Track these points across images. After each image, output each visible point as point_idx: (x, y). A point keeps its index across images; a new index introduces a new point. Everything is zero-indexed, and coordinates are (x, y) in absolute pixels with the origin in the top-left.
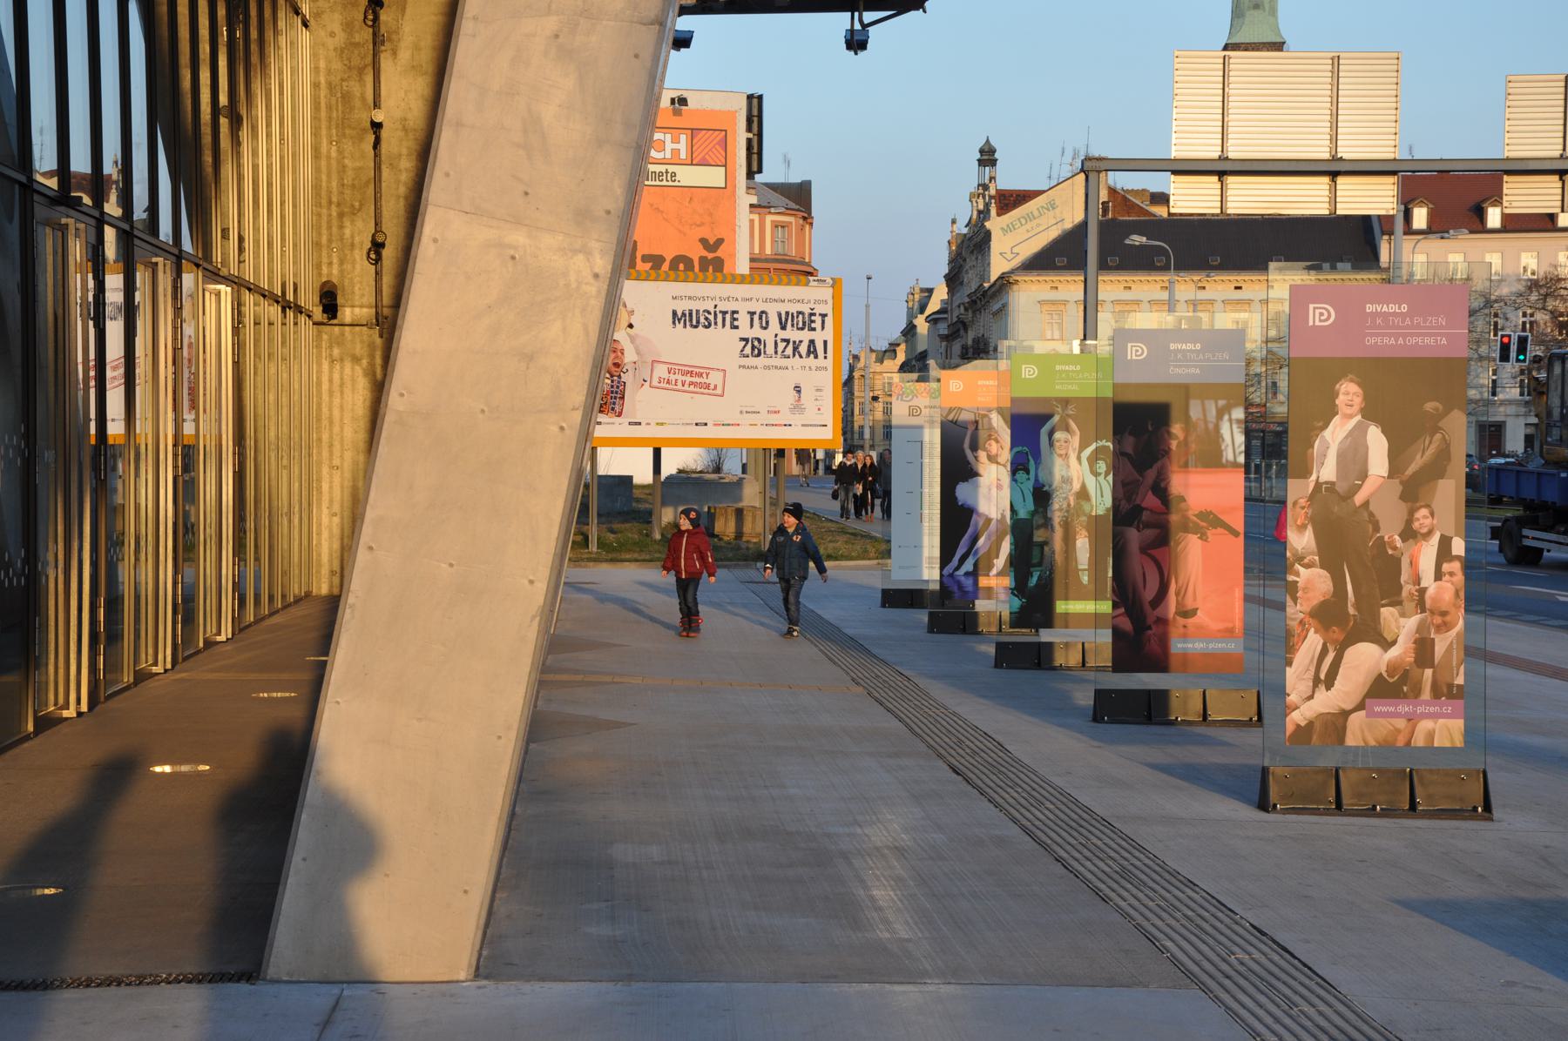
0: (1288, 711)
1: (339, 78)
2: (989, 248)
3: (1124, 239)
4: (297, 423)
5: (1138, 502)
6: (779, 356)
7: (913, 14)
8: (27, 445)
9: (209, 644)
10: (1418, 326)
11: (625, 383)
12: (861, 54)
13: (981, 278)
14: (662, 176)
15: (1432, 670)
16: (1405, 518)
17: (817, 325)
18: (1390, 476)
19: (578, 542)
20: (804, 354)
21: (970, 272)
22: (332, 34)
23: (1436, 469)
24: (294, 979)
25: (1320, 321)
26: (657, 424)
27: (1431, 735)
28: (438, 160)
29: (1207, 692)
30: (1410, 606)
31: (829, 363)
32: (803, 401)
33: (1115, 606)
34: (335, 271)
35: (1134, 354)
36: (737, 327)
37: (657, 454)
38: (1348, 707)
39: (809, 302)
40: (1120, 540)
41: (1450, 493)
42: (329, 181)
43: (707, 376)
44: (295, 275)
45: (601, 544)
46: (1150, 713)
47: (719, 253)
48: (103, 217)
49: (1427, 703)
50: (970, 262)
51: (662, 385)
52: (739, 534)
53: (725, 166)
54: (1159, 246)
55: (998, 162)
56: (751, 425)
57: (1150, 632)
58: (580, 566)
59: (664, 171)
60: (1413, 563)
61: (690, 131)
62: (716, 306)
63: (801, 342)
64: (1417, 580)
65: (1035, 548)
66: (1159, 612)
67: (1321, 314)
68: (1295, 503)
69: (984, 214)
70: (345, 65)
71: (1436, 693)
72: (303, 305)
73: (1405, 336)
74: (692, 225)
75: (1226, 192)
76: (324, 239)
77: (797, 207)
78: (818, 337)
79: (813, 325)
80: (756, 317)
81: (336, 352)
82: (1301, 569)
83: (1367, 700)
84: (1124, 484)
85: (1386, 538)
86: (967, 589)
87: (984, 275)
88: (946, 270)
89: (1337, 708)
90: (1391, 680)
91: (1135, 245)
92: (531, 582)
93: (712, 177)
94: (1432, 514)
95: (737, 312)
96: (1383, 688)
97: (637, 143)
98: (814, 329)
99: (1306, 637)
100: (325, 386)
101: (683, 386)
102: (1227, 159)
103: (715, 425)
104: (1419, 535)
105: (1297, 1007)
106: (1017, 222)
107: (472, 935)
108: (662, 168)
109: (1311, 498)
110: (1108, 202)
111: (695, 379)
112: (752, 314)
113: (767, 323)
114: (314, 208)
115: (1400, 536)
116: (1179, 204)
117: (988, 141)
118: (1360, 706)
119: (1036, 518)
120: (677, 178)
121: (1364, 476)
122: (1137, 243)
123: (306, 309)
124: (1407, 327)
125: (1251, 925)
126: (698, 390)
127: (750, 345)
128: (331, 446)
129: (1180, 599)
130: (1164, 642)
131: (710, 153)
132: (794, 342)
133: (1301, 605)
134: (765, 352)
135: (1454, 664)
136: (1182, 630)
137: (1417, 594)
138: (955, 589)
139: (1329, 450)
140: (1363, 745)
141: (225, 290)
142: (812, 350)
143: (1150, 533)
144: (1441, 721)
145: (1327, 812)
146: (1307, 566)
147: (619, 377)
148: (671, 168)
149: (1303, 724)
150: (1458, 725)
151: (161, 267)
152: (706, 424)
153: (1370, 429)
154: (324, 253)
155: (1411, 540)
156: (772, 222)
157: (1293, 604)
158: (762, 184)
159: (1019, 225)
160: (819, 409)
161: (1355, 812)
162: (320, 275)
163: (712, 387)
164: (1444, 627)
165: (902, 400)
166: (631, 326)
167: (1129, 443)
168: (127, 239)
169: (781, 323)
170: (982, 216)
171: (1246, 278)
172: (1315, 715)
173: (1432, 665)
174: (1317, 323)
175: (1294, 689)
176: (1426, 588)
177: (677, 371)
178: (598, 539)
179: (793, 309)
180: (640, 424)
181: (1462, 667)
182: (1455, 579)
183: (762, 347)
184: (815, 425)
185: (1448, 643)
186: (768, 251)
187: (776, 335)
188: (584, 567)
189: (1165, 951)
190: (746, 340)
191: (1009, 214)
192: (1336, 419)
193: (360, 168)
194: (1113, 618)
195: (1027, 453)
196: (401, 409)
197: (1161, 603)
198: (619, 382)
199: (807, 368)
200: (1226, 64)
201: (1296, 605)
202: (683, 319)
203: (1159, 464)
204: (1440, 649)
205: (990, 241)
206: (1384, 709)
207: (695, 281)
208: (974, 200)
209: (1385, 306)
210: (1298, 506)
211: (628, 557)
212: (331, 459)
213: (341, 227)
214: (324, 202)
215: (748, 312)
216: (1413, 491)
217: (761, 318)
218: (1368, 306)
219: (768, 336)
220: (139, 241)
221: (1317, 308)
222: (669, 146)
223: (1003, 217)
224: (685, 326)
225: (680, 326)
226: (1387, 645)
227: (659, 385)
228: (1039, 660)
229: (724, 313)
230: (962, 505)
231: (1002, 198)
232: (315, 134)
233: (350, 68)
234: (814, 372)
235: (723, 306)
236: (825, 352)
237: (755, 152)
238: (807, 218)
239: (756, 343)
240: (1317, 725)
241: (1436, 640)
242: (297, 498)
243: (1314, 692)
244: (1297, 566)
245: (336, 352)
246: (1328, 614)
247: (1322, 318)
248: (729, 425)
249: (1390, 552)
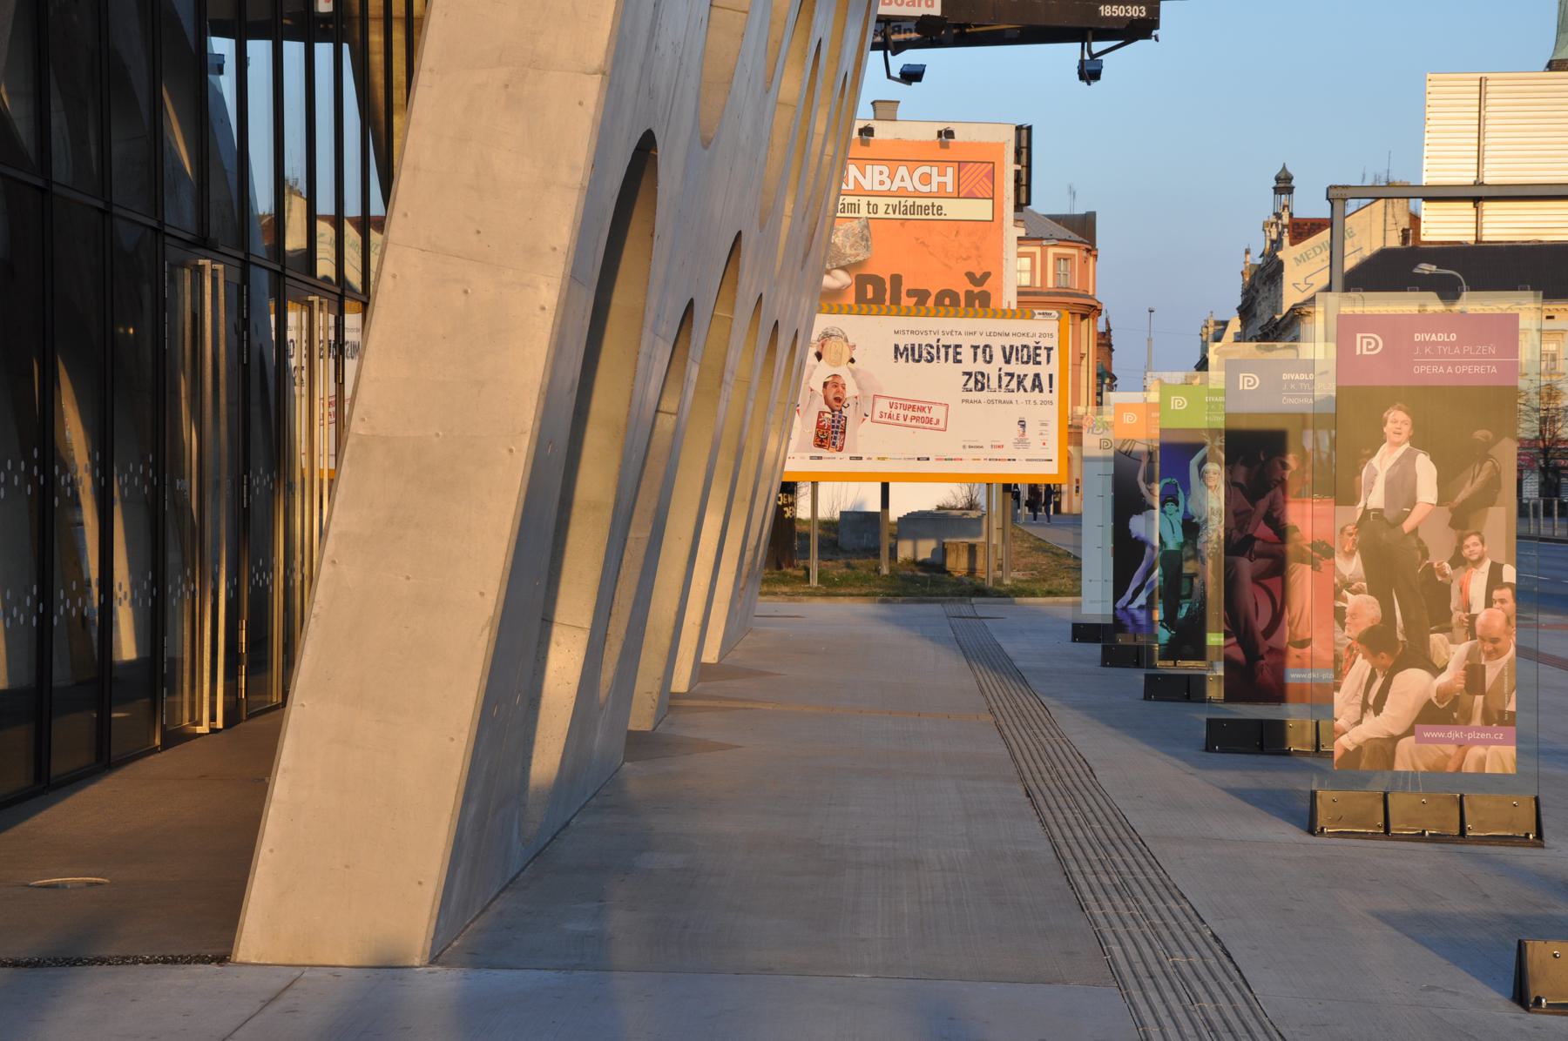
0: (1336, 736)
2: (1282, 278)
3: (1412, 269)
5: (1250, 532)
6: (1003, 390)
7: (1140, 43)
8: (156, 473)
10: (1468, 355)
11: (846, 418)
12: (1095, 84)
13: (1273, 310)
14: (929, 209)
15: (1482, 696)
16: (1455, 544)
17: (1043, 359)
18: (1440, 503)
19: (801, 577)
20: (1028, 388)
21: (1263, 304)
23: (1487, 497)
24: (262, 962)
25: (1368, 350)
26: (879, 458)
27: (1482, 762)
28: (396, 202)
29: (1320, 723)
30: (1459, 632)
31: (1055, 397)
32: (1026, 433)
33: (1226, 637)
35: (1246, 385)
36: (960, 361)
37: (885, 488)
38: (1398, 732)
39: (1034, 335)
40: (1231, 570)
41: (1500, 520)
43: (930, 410)
45: (821, 580)
46: (1262, 743)
47: (985, 287)
48: (249, 258)
49: (1478, 730)
50: (1263, 293)
51: (883, 419)
52: (972, 571)
53: (993, 198)
54: (1449, 275)
55: (1295, 190)
56: (974, 459)
57: (1262, 662)
58: (794, 601)
59: (930, 204)
60: (1463, 590)
61: (957, 164)
62: (938, 341)
63: (1025, 376)
64: (1467, 606)
65: (1184, 580)
66: (1273, 641)
67: (1369, 343)
68: (1343, 530)
69: (1276, 244)
71: (1487, 719)
73: (1454, 365)
74: (957, 259)
75: (1482, 219)
77: (1081, 239)
78: (1044, 369)
79: (1038, 359)
80: (980, 351)
82: (1349, 595)
83: (1416, 726)
84: (1236, 515)
85: (1435, 565)
86: (1140, 623)
87: (1276, 308)
88: (1239, 302)
89: (1386, 733)
90: (1441, 706)
91: (1424, 274)
92: (482, 594)
93: (979, 209)
94: (1482, 542)
95: (960, 346)
96: (1433, 714)
97: (582, 184)
98: (1039, 363)
99: (1354, 662)
101: (905, 420)
102: (1482, 184)
103: (937, 459)
104: (1469, 563)
105: (1198, 1003)
106: (1312, 252)
107: (426, 925)
108: (928, 202)
109: (1359, 525)
110: (1408, 230)
111: (917, 413)
112: (976, 348)
113: (991, 356)
115: (1449, 562)
116: (1430, 231)
117: (1284, 168)
118: (1410, 732)
119: (1185, 549)
120: (943, 212)
121: (1413, 503)
122: (1427, 272)
124: (1456, 356)
125: (1213, 935)
126: (921, 424)
127: (973, 379)
129: (1293, 629)
130: (1279, 671)
131: (981, 183)
132: (1019, 376)
133: (1350, 631)
134: (988, 386)
135: (1506, 690)
136: (1296, 661)
137: (1467, 620)
138: (1128, 622)
139: (1377, 478)
140: (1413, 770)
142: (1037, 383)
143: (1262, 563)
144: (1493, 748)
145: (1374, 836)
146: (1355, 592)
147: (841, 411)
148: (937, 202)
149: (1351, 748)
150: (1509, 751)
151: (316, 305)
152: (928, 459)
153: (1418, 456)
155: (1461, 567)
156: (1055, 254)
157: (1341, 630)
158: (1052, 218)
159: (1313, 254)
160: (1044, 444)
161: (1403, 837)
163: (934, 421)
164: (1495, 654)
165: (1093, 433)
166: (852, 361)
167: (1241, 474)
168: (279, 278)
169: (1005, 356)
170: (1275, 245)
171: (1559, 307)
172: (1363, 740)
173: (1483, 692)
174: (1365, 352)
175: (1342, 714)
176: (1476, 615)
177: (899, 406)
178: (819, 575)
179: (1018, 342)
180: (861, 458)
181: (1514, 694)
182: (1506, 606)
183: (986, 381)
184: (1040, 460)
185: (1500, 670)
186: (1050, 284)
187: (1000, 369)
188: (798, 601)
189: (1107, 953)
190: (969, 374)
191: (1301, 245)
192: (1384, 448)
194: (1225, 647)
195: (1176, 484)
196: (362, 432)
197: (1276, 628)
198: (840, 417)
199: (1032, 402)
200: (1483, 86)
201: (1344, 629)
202: (905, 353)
203: (1272, 493)
204: (1491, 675)
205: (1282, 271)
206: (1434, 735)
207: (975, 316)
208: (1267, 229)
209: (1434, 335)
210: (1345, 534)
211: (843, 591)
215: (972, 346)
216: (1462, 519)
217: (984, 352)
218: (1416, 335)
219: (991, 370)
220: (290, 280)
221: (1365, 337)
222: (936, 179)
223: (1296, 246)
224: (907, 361)
225: (902, 360)
226: (1436, 671)
227: (880, 419)
228: (1188, 692)
229: (947, 347)
230: (1136, 538)
231: (1296, 227)
234: (1039, 406)
235: (944, 341)
236: (1051, 386)
237: (1023, 184)
238: (1091, 250)
239: (979, 377)
240: (1366, 751)
241: (1487, 667)
243: (1362, 717)
244: (1345, 592)
246: (1376, 640)
247: (1370, 347)
248: (952, 460)
249: (1439, 579)
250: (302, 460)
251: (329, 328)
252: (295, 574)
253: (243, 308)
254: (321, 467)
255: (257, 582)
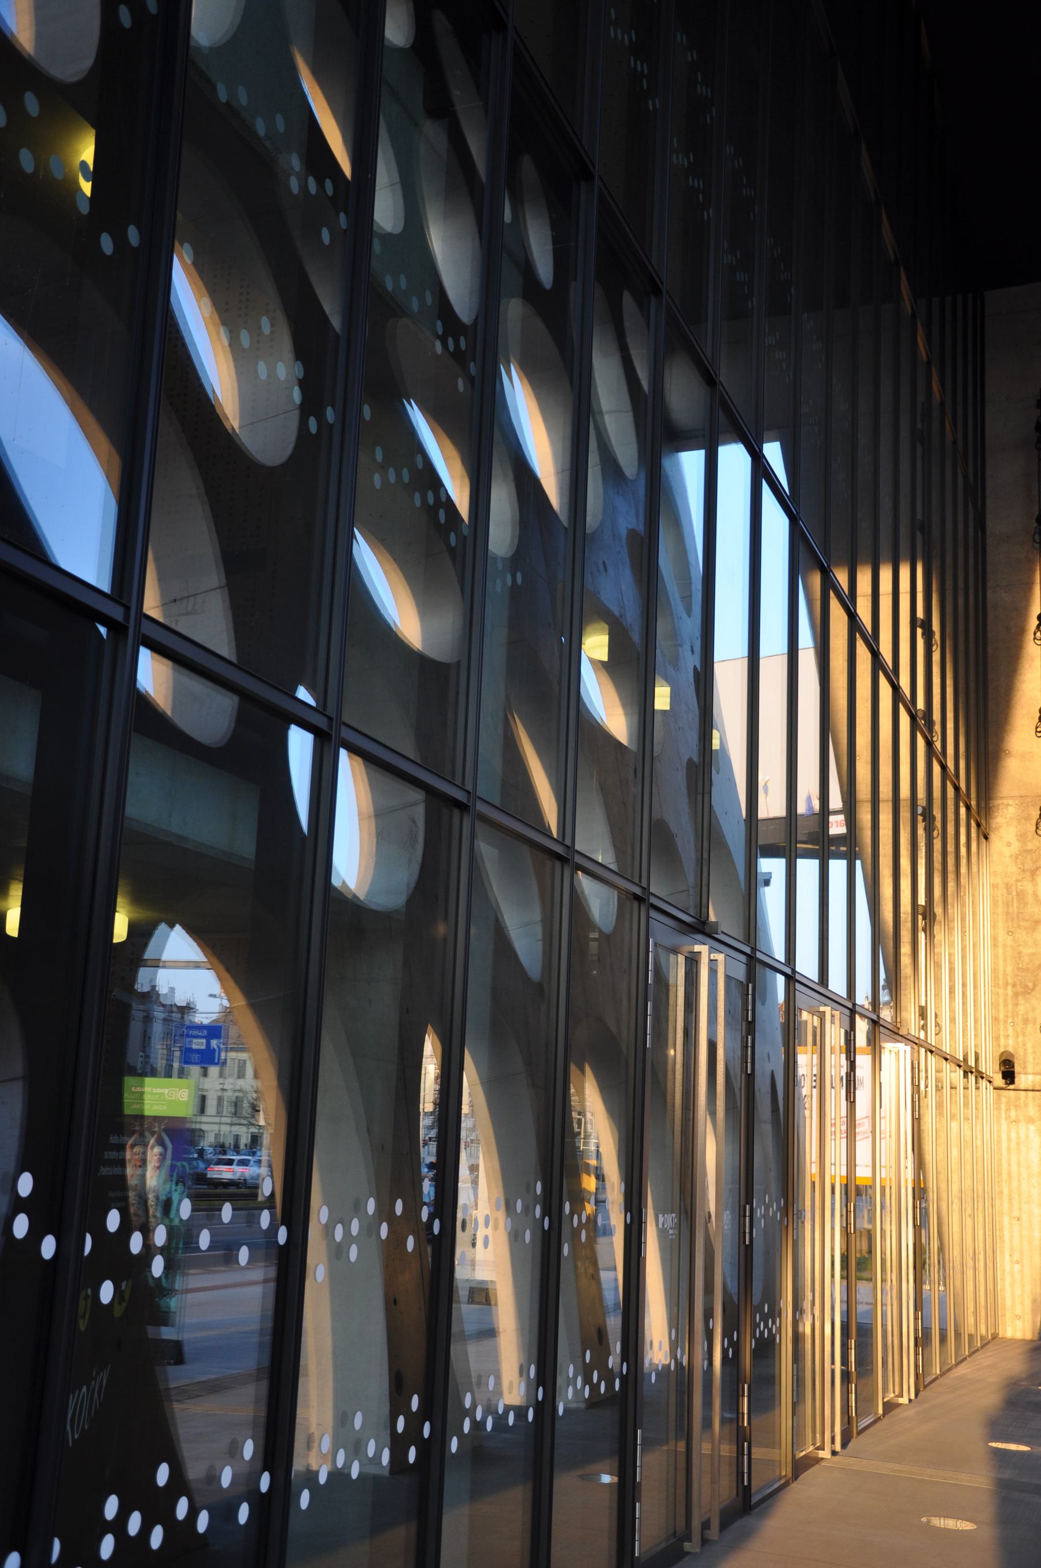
1: (1015, 879)
4: (980, 1176)
9: (889, 1407)
22: (1009, 844)
34: (1011, 1042)
42: (1005, 966)
44: (976, 1046)
70: (1020, 868)
72: (984, 1071)
76: (1001, 1016)
81: (1013, 1114)
100: (1004, 1145)
114: (993, 988)
123: (986, 1075)
128: (1010, 1199)
141: (903, 1049)
154: (1002, 1027)
162: (999, 1046)
193: (1034, 954)
212: (1011, 1210)
213: (1017, 1005)
214: (1001, 983)
232: (994, 927)
233: (1023, 871)
242: (981, 1245)
245: (1013, 1114)
250: (812, 1168)
251: (841, 1066)
252: (805, 1316)
253: (747, 1010)
254: (833, 1174)
255: (762, 1333)
